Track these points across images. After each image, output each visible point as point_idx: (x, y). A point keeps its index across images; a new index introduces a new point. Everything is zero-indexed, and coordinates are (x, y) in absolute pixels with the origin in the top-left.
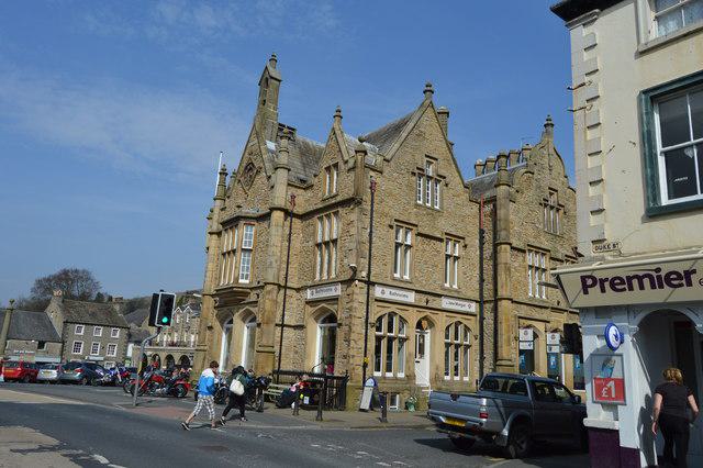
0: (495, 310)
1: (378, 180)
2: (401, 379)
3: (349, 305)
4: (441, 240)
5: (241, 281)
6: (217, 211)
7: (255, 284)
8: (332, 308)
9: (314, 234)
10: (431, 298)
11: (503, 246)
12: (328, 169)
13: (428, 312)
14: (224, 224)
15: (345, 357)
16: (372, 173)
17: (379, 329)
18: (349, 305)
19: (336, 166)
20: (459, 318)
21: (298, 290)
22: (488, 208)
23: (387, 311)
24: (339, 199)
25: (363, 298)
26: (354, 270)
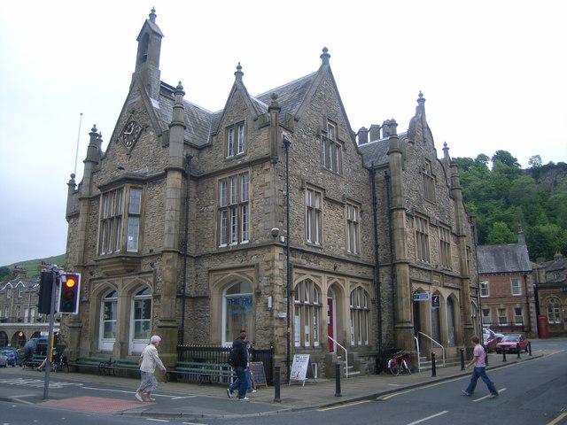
0: (393, 276)
1: (290, 140)
2: (317, 348)
3: (268, 273)
9: (216, 197)
10: (338, 264)
11: (400, 212)
12: (230, 128)
13: (336, 279)
15: (266, 328)
16: (284, 133)
18: (268, 273)
19: (240, 124)
21: (198, 258)
22: (380, 175)
23: (303, 278)
24: (246, 159)
25: (280, 265)
26: (275, 235)
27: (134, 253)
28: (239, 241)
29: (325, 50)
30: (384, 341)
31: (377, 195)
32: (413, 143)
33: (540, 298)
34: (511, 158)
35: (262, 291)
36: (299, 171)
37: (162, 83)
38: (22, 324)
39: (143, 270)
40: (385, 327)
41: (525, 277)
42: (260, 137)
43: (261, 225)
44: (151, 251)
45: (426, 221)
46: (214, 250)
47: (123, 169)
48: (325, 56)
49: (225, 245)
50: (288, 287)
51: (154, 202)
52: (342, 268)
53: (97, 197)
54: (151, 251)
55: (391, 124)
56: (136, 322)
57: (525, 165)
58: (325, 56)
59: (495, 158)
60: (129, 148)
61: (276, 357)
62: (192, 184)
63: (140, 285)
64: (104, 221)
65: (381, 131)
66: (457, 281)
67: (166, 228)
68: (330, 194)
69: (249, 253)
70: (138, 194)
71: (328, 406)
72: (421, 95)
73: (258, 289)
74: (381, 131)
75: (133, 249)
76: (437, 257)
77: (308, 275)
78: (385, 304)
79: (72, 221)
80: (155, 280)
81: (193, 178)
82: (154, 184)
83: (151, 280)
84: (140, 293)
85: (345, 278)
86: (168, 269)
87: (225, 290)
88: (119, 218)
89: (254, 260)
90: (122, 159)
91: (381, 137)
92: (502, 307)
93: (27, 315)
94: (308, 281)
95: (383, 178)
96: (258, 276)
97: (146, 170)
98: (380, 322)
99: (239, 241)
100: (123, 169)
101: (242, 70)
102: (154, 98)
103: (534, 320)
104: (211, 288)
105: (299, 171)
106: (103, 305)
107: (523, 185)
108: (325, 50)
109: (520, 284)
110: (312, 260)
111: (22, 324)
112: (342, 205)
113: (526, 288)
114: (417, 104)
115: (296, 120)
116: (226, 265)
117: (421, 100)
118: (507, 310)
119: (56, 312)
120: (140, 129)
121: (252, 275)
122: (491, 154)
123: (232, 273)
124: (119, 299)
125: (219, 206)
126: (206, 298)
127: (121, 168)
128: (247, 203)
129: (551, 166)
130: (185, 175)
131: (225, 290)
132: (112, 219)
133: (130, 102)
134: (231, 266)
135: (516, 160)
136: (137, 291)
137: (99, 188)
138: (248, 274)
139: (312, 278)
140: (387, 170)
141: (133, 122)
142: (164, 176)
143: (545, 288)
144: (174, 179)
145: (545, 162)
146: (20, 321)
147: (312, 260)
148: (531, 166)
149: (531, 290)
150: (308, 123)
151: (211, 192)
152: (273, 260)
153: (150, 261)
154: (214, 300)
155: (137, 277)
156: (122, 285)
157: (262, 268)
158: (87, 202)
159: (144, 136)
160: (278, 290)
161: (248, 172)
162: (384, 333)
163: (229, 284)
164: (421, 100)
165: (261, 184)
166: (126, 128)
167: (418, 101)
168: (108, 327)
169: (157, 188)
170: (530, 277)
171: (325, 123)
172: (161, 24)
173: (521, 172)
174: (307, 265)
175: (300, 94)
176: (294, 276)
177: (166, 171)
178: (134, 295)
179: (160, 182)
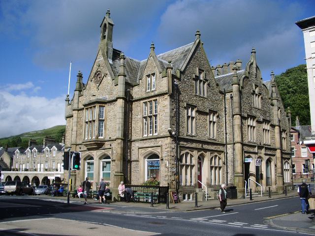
4: (206, 114)
5: (100, 137)
6: (76, 97)
7: (107, 138)
8: (157, 151)
12: (148, 76)
13: (202, 152)
14: (85, 105)
17: (181, 162)
19: (153, 74)
20: (216, 154)
23: (214, 154)
24: (156, 93)
30: (229, 182)
31: (227, 107)
39: (106, 147)
40: (229, 175)
43: (163, 126)
44: (110, 138)
46: (141, 138)
47: (95, 96)
49: (151, 135)
50: (177, 156)
52: (205, 147)
53: (82, 109)
54: (110, 138)
56: (88, 173)
67: (118, 128)
68: (201, 109)
71: (188, 211)
77: (187, 151)
80: (112, 152)
83: (110, 152)
87: (147, 157)
89: (160, 144)
93: (39, 167)
97: (108, 98)
99: (153, 133)
100: (95, 96)
102: (110, 58)
104: (140, 157)
106: (86, 164)
119: (71, 169)
124: (96, 161)
127: (94, 96)
128: (157, 115)
131: (147, 157)
132: (90, 122)
134: (149, 146)
139: (189, 152)
153: (109, 143)
156: (96, 154)
162: (229, 179)
168: (156, 131)
169: (112, 106)
175: (184, 56)
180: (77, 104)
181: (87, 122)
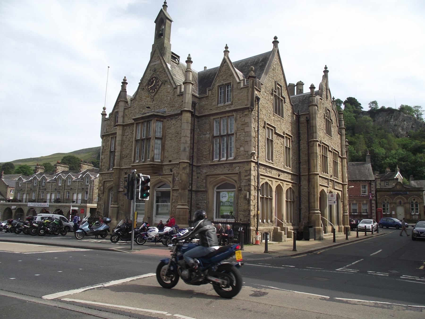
3: (247, 178)
13: (279, 182)
18: (247, 178)
23: (264, 181)
27: (159, 162)
28: (227, 157)
29: (276, 38)
32: (321, 99)
33: (378, 197)
34: (357, 102)
35: (243, 189)
36: (263, 116)
37: (173, 53)
38: (22, 203)
41: (370, 184)
42: (242, 94)
43: (242, 149)
45: (289, 139)
48: (275, 42)
51: (172, 130)
53: (133, 124)
55: (300, 84)
57: (366, 108)
58: (275, 42)
59: (345, 103)
60: (153, 94)
61: (251, 228)
62: (196, 120)
63: (162, 182)
64: (137, 141)
65: (296, 87)
66: (341, 186)
69: (234, 165)
70: (160, 124)
72: (326, 68)
73: (240, 187)
74: (296, 87)
75: (158, 160)
76: (332, 171)
77: (267, 180)
78: (304, 200)
79: (105, 138)
81: (198, 117)
82: (172, 119)
83: (171, 179)
84: (158, 188)
85: (283, 182)
86: (183, 173)
88: (148, 139)
90: (146, 100)
91: (295, 94)
92: (355, 202)
94: (267, 183)
95: (305, 121)
96: (240, 179)
97: (168, 111)
98: (300, 210)
101: (228, 49)
103: (374, 211)
105: (263, 116)
107: (366, 121)
108: (276, 38)
109: (367, 188)
110: (268, 170)
111: (22, 203)
112: (283, 137)
113: (370, 191)
114: (323, 74)
115: (262, 84)
116: (218, 172)
117: (326, 71)
118: (358, 205)
120: (160, 83)
121: (236, 178)
122: (344, 99)
123: (222, 177)
125: (213, 135)
126: (206, 191)
129: (383, 109)
130: (193, 115)
132: (142, 140)
133: (152, 64)
135: (360, 104)
136: (159, 185)
137: (133, 119)
138: (233, 178)
140: (308, 116)
141: (156, 77)
142: (181, 113)
143: (381, 191)
144: (187, 117)
145: (380, 107)
146: (20, 201)
147: (268, 170)
148: (370, 109)
149: (374, 192)
150: (268, 86)
151: (207, 126)
152: (250, 170)
153: (170, 167)
154: (210, 192)
155: (160, 177)
157: (243, 175)
158: (121, 128)
159: (163, 87)
160: (252, 188)
161: (233, 115)
163: (217, 184)
164: (326, 71)
165: (243, 123)
166: (150, 82)
167: (324, 72)
169: (173, 122)
170: (373, 183)
171: (275, 85)
172: (170, 13)
173: (364, 113)
174: (266, 174)
176: (260, 180)
177: (182, 112)
178: (155, 188)
179: (176, 118)
180: (122, 118)
181: (137, 141)
